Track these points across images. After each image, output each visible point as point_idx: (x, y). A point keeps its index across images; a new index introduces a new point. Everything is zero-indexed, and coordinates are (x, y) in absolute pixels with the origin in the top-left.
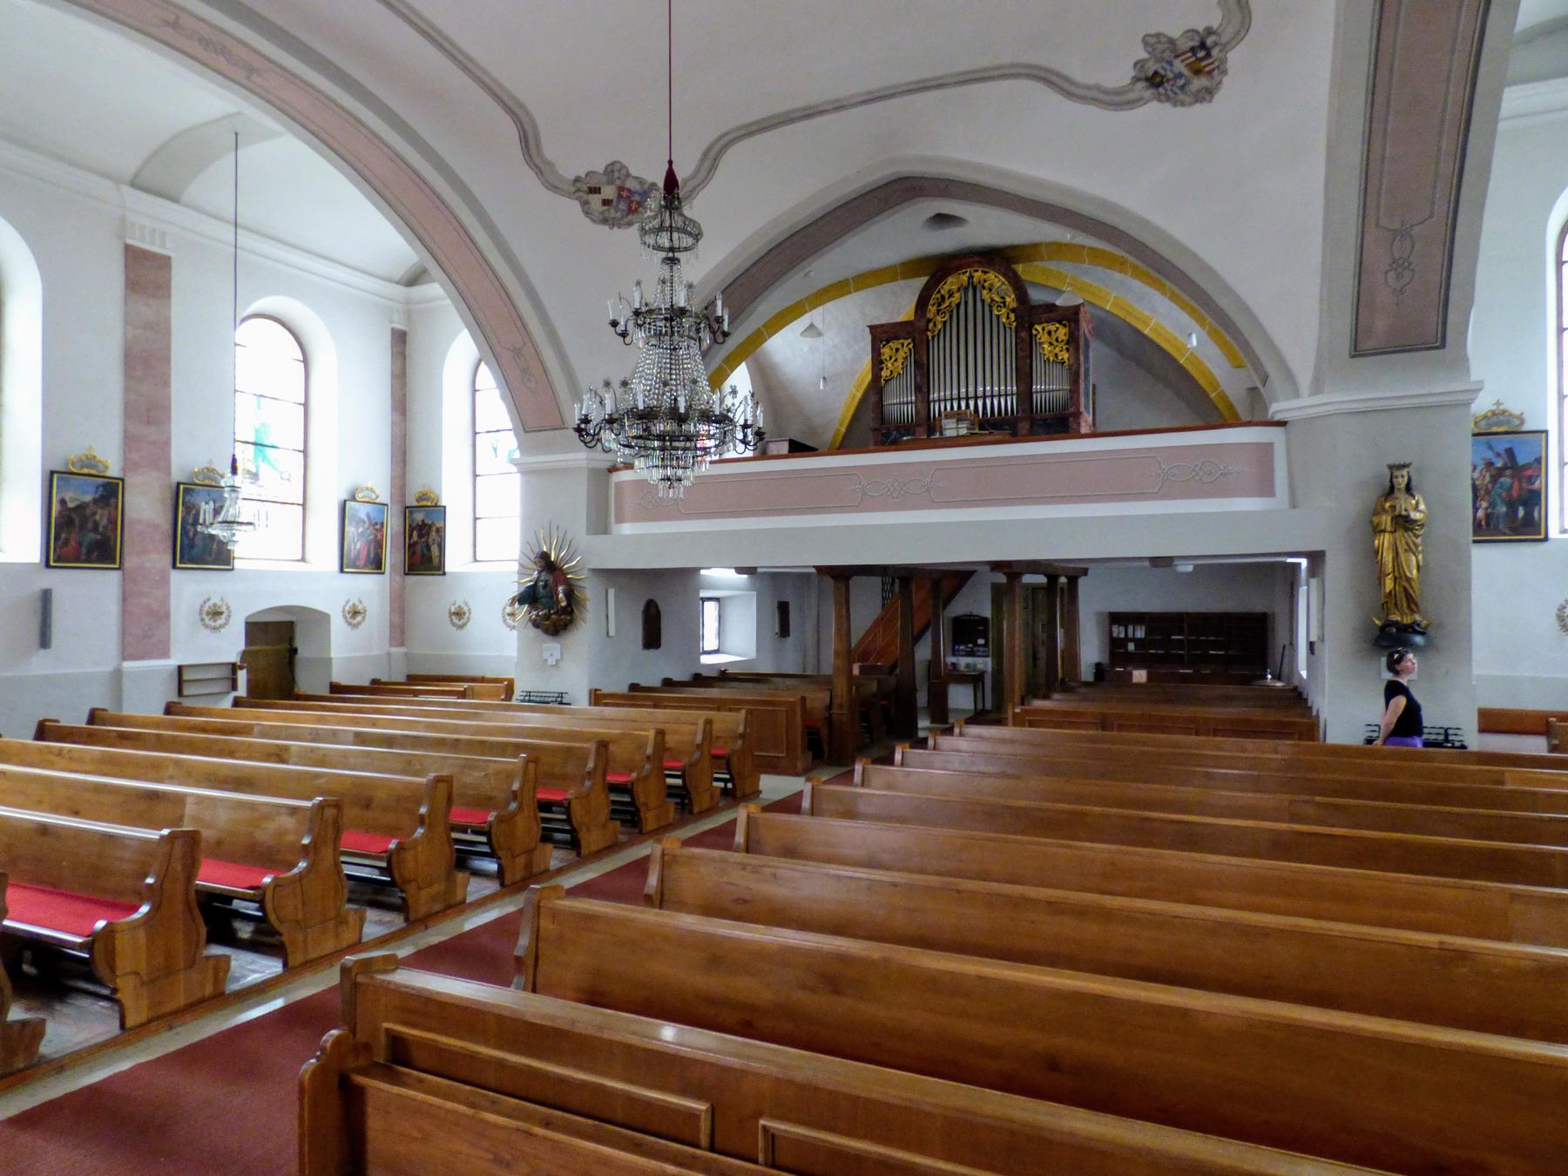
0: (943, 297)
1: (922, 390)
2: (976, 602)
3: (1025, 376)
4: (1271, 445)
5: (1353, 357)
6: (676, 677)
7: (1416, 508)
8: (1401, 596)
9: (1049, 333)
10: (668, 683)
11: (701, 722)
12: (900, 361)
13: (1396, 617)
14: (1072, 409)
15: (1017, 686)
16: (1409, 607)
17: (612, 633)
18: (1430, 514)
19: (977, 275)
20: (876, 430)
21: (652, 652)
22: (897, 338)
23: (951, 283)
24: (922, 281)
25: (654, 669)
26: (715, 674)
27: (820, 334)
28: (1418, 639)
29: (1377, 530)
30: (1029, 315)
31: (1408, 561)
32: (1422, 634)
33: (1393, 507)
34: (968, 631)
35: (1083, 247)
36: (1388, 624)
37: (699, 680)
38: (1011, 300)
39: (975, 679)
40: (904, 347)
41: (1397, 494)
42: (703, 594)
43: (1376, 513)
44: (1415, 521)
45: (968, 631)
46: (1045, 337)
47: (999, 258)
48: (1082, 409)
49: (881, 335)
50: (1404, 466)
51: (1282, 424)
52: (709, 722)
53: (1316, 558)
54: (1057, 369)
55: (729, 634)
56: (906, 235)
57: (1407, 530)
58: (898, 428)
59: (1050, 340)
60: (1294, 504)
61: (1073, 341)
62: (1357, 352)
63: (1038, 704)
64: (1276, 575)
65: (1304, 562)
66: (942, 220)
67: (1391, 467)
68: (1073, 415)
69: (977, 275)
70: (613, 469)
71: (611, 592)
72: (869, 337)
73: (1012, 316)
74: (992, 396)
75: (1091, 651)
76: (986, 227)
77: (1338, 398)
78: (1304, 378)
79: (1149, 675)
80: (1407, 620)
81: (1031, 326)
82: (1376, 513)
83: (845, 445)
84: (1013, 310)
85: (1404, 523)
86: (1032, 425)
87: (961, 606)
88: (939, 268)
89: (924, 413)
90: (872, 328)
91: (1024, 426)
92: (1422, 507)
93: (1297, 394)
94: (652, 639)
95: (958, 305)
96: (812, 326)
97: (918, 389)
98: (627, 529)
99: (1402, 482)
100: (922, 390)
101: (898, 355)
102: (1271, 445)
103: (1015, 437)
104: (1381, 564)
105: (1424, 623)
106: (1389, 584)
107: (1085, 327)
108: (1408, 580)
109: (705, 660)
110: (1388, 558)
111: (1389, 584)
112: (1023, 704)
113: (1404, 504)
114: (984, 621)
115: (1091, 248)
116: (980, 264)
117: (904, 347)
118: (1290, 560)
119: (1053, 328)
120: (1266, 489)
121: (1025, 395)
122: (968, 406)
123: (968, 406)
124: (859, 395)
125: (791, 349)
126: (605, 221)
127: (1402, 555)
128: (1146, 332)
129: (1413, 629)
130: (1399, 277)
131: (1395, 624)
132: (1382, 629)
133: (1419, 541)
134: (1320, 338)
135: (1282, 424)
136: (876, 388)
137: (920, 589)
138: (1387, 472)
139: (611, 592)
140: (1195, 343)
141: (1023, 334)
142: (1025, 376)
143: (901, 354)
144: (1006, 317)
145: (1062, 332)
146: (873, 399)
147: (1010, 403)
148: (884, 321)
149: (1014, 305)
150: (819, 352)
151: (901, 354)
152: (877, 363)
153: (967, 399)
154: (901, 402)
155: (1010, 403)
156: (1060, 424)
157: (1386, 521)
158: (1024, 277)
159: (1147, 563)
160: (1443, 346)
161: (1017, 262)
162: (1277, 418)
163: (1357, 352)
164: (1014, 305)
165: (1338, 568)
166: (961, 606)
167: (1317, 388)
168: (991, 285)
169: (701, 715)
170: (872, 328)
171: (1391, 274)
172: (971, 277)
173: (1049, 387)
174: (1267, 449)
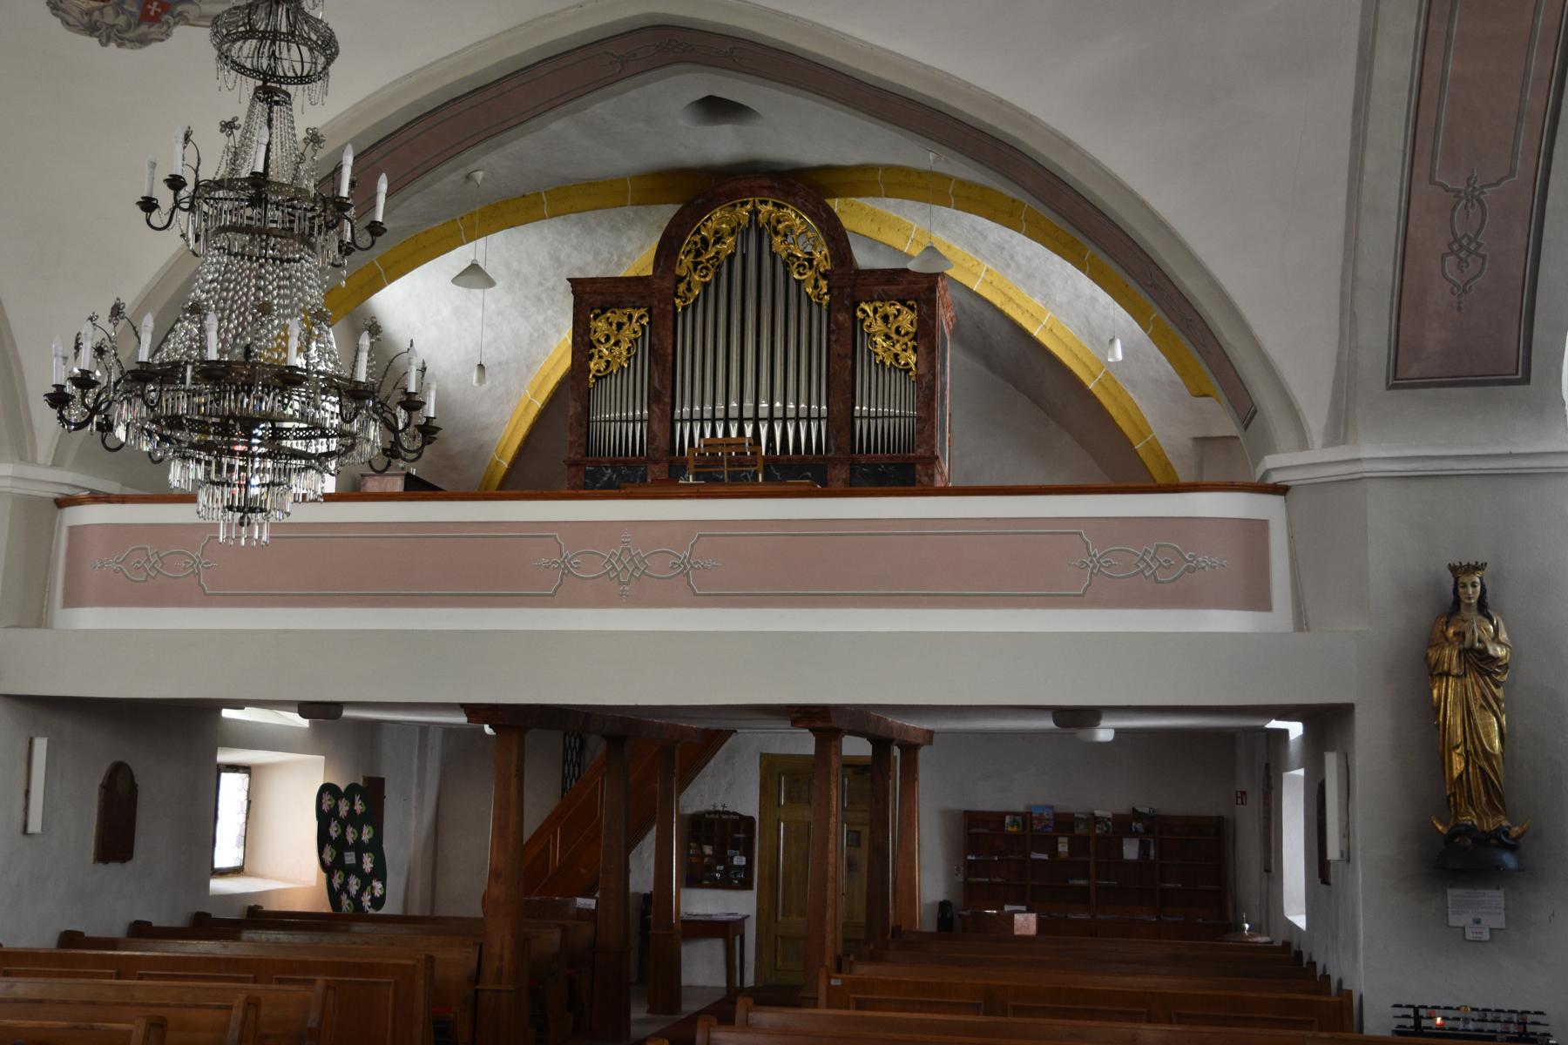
0: (704, 240)
1: (662, 397)
2: (730, 787)
3: (841, 390)
4: (1263, 525)
5: (1390, 387)
6: (157, 922)
7: (1495, 639)
8: (1476, 781)
9: (885, 318)
10: (141, 930)
11: (238, 1001)
12: (625, 346)
13: (1470, 819)
14: (920, 451)
15: (829, 938)
16: (1490, 802)
17: (35, 826)
18: (1512, 647)
19: (765, 209)
20: (572, 464)
21: (113, 868)
22: (620, 305)
23: (717, 219)
24: (668, 211)
25: (117, 901)
26: (235, 914)
27: (490, 283)
28: (1509, 860)
29: (1436, 672)
30: (852, 285)
31: (1487, 725)
32: (1513, 848)
33: (1460, 635)
34: (718, 846)
35: (949, 178)
36: (1459, 831)
37: (204, 925)
38: (821, 254)
39: (726, 930)
40: (635, 323)
41: (1465, 613)
42: (224, 756)
43: (1432, 644)
44: (1496, 659)
45: (718, 846)
46: (878, 326)
47: (810, 187)
48: (937, 452)
49: (592, 298)
50: (1478, 568)
51: (1280, 490)
52: (253, 1004)
53: (1327, 723)
54: (897, 377)
55: (267, 836)
56: (663, 124)
57: (1484, 672)
58: (614, 465)
59: (886, 330)
60: (1301, 620)
61: (925, 335)
62: (1398, 380)
63: (863, 970)
64: (1226, 753)
65: (1295, 729)
66: (715, 109)
67: (1453, 569)
68: (921, 459)
69: (765, 209)
70: (63, 502)
71: (41, 745)
72: (568, 302)
73: (823, 283)
74: (797, 419)
75: (932, 880)
76: (795, 132)
77: (1374, 451)
78: (1316, 419)
79: (1040, 924)
80: (1489, 825)
81: (856, 305)
82: (1432, 644)
83: (520, 480)
84: (825, 276)
85: (1479, 661)
86: (852, 471)
87: (699, 797)
88: (694, 191)
89: (662, 441)
90: (578, 285)
91: (840, 473)
92: (1503, 636)
93: (1304, 445)
94: (115, 841)
95: (731, 257)
96: (474, 269)
97: (654, 397)
98: (89, 618)
99: (1474, 593)
100: (662, 397)
101: (620, 339)
102: (1263, 525)
103: (822, 487)
104: (1443, 728)
105: (1516, 830)
106: (1458, 765)
107: (945, 317)
108: (1488, 756)
109: (218, 885)
110: (1455, 719)
111: (1458, 765)
112: (839, 970)
113: (1481, 630)
114: (749, 821)
115: (962, 183)
116: (771, 190)
117: (635, 323)
118: (1275, 724)
119: (891, 310)
120: (1258, 599)
121: (842, 420)
122: (741, 432)
123: (741, 432)
124: (538, 404)
125: (426, 311)
126: (91, 29)
127: (1477, 714)
128: (1036, 332)
129: (1501, 841)
130: (1461, 263)
131: (1469, 830)
132: (1449, 838)
133: (1500, 693)
134: (1340, 354)
135: (1280, 490)
136: (575, 390)
137: (624, 757)
138: (1449, 578)
139: (41, 745)
140: (1120, 356)
141: (842, 317)
142: (841, 390)
143: (627, 334)
144: (813, 286)
145: (907, 320)
146: (573, 408)
147: (815, 432)
148: (594, 272)
149: (826, 266)
150: (474, 323)
151: (627, 334)
152: (583, 345)
153: (727, 420)
154: (621, 418)
155: (815, 432)
156: (903, 470)
157: (1450, 656)
158: (847, 223)
159: (1048, 723)
160: (1526, 380)
161: (835, 196)
162: (1275, 478)
163: (1398, 380)
164: (826, 266)
165: (1372, 734)
166: (699, 797)
167: (1339, 429)
168: (790, 229)
169: (238, 992)
170: (578, 285)
171: (1451, 259)
172: (755, 212)
173: (881, 409)
174: (1256, 530)
